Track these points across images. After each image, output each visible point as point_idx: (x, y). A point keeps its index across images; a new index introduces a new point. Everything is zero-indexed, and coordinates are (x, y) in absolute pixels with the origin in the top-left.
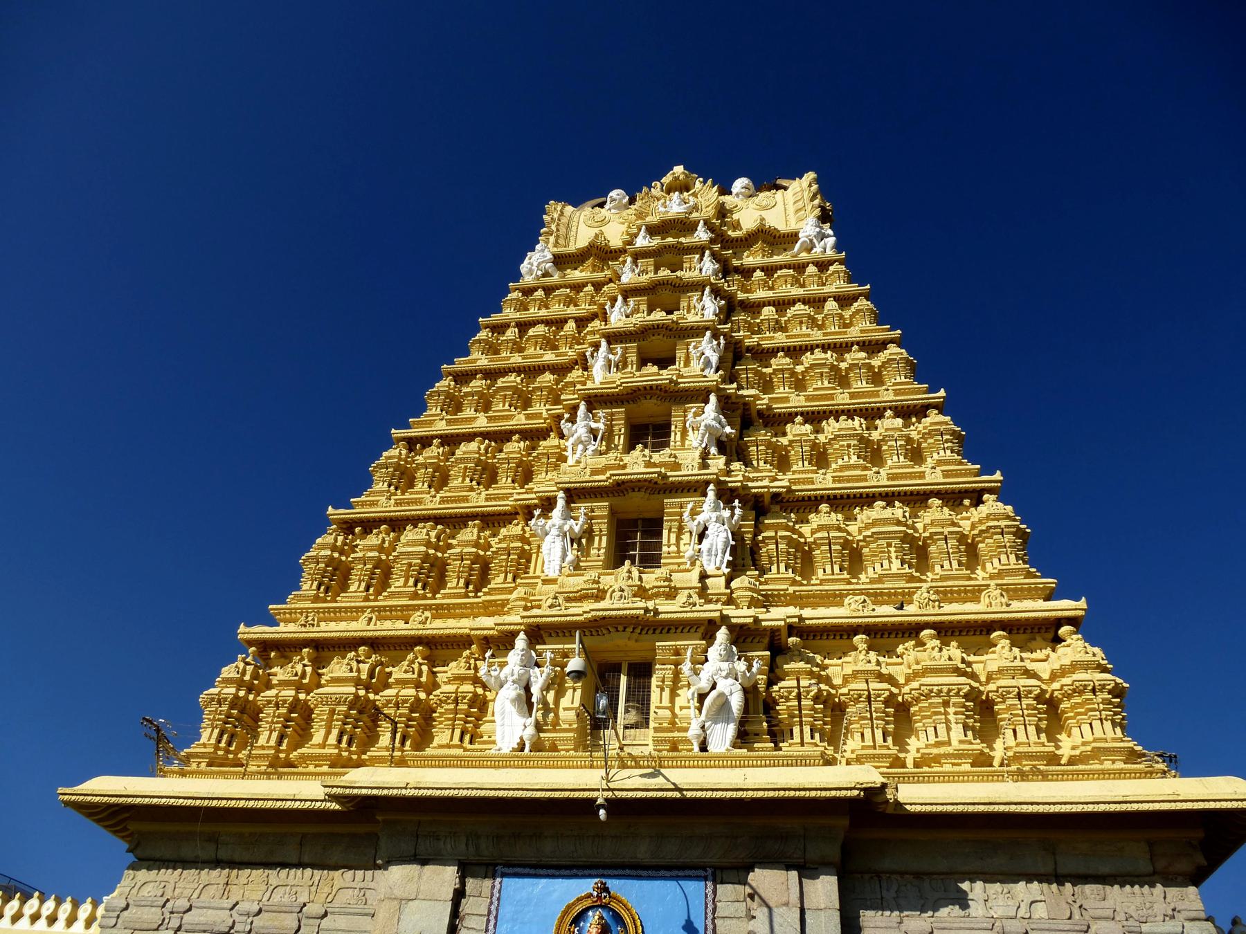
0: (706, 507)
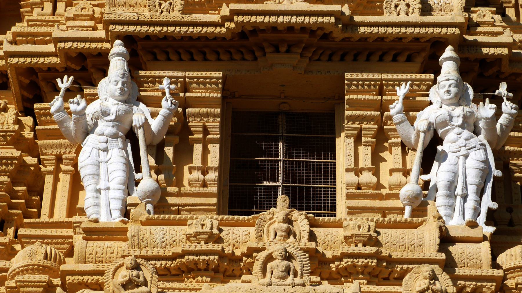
0: (437, 94)
